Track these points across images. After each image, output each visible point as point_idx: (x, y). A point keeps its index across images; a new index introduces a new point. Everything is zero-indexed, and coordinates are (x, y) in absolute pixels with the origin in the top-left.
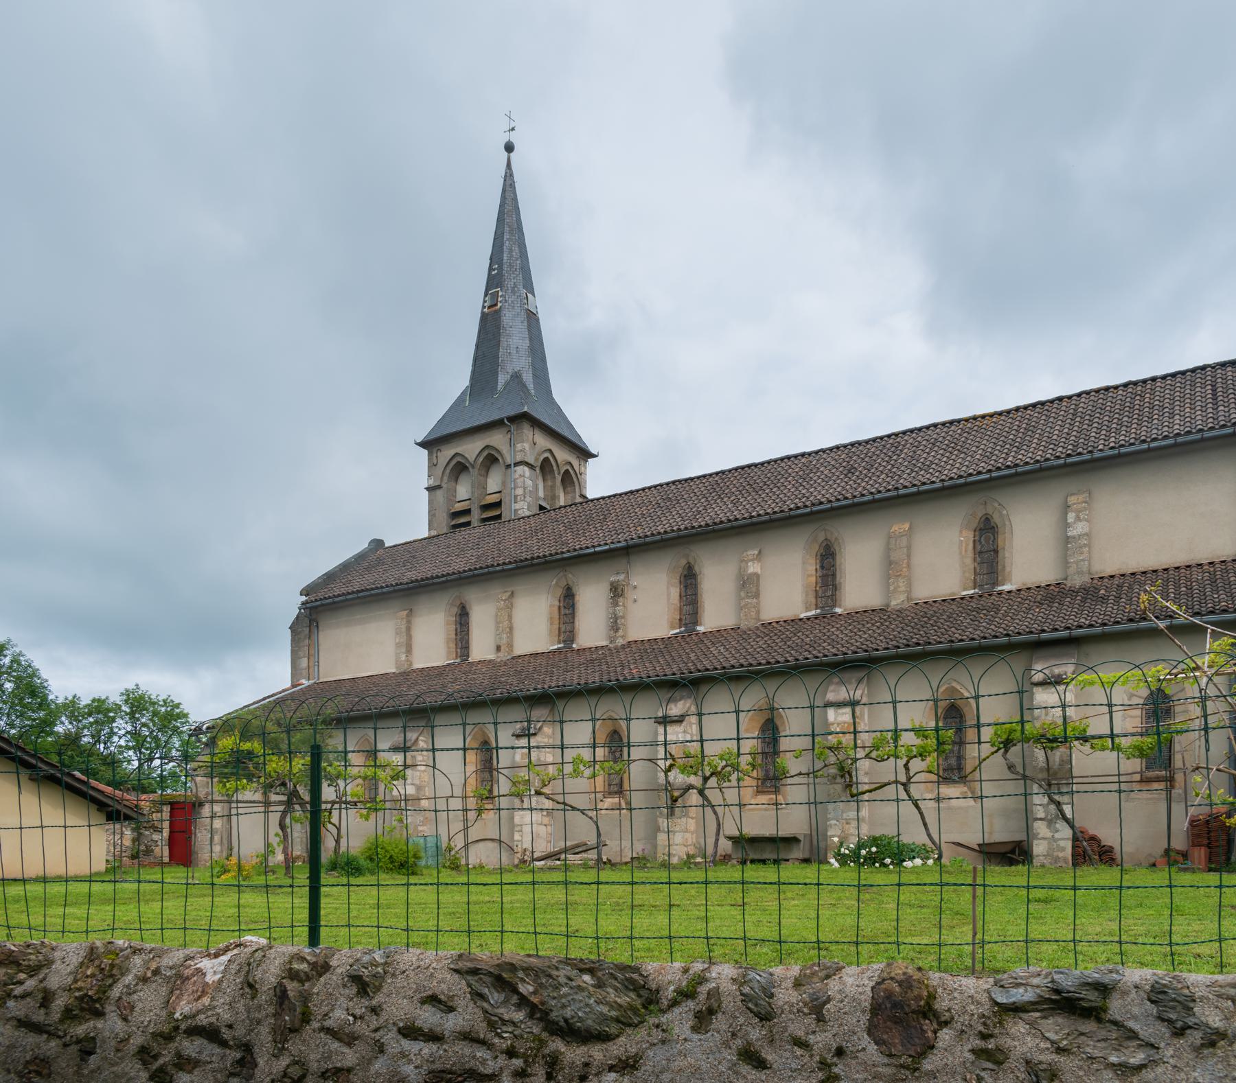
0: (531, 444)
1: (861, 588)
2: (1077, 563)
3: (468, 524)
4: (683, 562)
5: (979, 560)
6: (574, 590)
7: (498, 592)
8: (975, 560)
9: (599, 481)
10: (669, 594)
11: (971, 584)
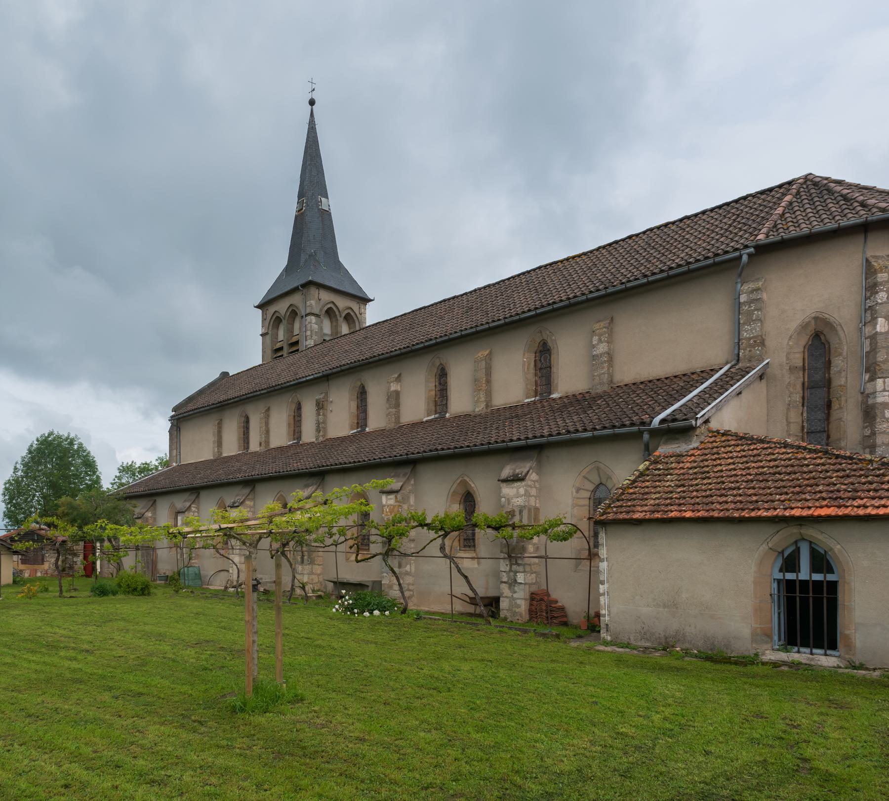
0: (317, 300)
1: (571, 378)
2: (599, 376)
4: (359, 384)
6: (550, 343)
7: (262, 406)
8: (536, 375)
9: (372, 315)
10: (350, 407)
11: (533, 394)
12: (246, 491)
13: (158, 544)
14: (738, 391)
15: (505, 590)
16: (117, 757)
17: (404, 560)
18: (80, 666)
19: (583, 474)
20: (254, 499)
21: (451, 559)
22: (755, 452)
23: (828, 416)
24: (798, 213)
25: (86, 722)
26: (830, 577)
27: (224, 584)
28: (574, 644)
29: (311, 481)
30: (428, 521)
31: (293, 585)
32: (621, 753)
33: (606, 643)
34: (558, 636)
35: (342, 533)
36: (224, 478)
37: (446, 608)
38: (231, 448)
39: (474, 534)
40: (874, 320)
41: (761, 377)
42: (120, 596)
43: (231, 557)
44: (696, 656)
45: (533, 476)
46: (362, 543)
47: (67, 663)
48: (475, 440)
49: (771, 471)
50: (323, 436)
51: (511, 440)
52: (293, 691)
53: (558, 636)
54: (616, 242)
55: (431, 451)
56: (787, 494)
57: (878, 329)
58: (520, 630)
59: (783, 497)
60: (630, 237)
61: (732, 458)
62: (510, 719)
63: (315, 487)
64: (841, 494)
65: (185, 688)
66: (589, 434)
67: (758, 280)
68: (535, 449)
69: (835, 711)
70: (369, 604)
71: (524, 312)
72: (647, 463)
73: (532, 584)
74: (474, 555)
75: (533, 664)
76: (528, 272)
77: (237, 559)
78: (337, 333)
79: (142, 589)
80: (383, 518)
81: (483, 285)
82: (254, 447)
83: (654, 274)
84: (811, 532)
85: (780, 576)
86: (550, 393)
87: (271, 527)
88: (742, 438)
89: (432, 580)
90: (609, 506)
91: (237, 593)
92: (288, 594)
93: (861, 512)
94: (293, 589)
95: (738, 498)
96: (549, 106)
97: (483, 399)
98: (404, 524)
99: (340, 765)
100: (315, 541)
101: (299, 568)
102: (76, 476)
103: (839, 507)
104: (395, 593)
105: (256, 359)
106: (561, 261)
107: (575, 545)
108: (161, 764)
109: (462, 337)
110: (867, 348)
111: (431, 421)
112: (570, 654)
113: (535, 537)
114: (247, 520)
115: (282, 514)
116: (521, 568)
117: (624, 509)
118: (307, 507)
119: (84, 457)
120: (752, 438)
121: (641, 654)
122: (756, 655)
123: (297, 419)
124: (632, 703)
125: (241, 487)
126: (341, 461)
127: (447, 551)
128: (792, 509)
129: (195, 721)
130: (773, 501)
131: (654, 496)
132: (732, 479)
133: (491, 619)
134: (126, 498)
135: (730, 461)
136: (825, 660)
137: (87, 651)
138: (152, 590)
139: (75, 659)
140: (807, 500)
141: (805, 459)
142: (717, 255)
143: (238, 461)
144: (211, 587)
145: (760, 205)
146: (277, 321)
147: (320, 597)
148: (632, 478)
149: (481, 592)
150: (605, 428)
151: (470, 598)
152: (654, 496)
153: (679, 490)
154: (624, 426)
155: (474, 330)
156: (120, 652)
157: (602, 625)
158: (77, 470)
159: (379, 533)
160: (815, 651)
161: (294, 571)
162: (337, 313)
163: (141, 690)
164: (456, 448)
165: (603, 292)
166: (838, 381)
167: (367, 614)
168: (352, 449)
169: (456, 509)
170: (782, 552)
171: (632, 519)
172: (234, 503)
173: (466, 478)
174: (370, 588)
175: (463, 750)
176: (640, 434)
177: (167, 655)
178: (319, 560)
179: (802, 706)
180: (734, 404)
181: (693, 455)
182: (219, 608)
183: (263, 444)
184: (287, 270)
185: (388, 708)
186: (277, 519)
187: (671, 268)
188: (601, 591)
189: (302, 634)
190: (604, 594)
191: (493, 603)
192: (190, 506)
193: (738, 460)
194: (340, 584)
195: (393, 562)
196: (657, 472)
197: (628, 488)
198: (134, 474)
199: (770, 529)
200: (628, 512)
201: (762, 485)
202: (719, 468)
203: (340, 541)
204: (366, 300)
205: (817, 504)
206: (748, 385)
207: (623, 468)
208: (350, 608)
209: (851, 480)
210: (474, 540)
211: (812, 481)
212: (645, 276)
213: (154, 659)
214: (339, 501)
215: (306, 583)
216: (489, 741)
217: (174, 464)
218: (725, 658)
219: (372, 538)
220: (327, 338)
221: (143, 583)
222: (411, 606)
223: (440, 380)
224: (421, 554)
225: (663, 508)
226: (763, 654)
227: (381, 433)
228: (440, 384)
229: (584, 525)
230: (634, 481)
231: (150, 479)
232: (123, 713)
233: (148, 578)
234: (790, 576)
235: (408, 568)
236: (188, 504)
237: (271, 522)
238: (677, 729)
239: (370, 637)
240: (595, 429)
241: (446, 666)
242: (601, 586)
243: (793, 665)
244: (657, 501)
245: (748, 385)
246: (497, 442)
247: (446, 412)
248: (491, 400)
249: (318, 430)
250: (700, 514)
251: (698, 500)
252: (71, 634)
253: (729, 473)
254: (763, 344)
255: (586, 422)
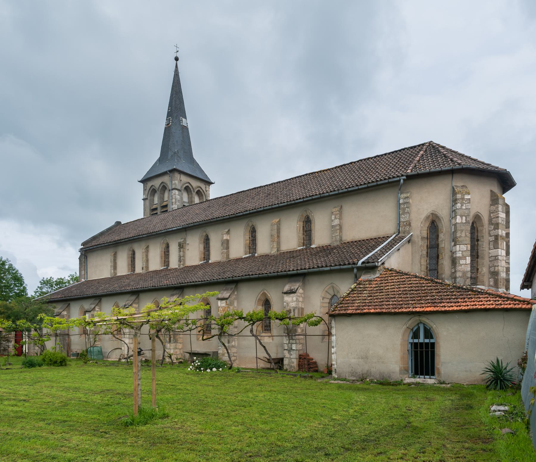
0: (179, 181)
2: (335, 237)
3: (157, 213)
4: (205, 234)
5: (305, 234)
6: (311, 217)
7: (143, 245)
8: (303, 234)
9: (214, 193)
10: (199, 247)
11: (302, 245)
12: (133, 298)
13: (71, 333)
14: (398, 248)
15: (286, 353)
16: (53, 454)
17: (231, 339)
18: (20, 409)
19: (326, 289)
20: (138, 303)
21: (256, 336)
22: (403, 280)
23: (438, 262)
24: (425, 161)
25: (29, 438)
26: (432, 341)
27: (118, 357)
28: (319, 381)
29: (175, 292)
30: (244, 316)
31: (163, 356)
32: (332, 427)
33: (335, 379)
34: (311, 377)
35: (194, 323)
36: (118, 290)
37: (254, 366)
38: (123, 270)
39: (270, 323)
40: (455, 217)
41: (409, 242)
42: (44, 367)
43: (123, 339)
44: (376, 383)
45: (301, 291)
46: (206, 330)
47: (11, 408)
48: (270, 270)
49: (409, 289)
50: (183, 265)
51: (289, 271)
52: (162, 412)
53: (311, 377)
54: (345, 165)
55: (246, 275)
56: (415, 300)
57: (457, 221)
58: (293, 375)
59: (413, 302)
60: (351, 163)
61: (393, 282)
62: (280, 417)
63: (178, 296)
64: (436, 301)
65: (95, 416)
66: (328, 268)
67: (408, 192)
68: (302, 276)
69: (427, 402)
70: (210, 365)
71: (297, 199)
72: (355, 284)
73: (300, 350)
74: (270, 335)
75: (297, 391)
76: (300, 176)
77: (127, 341)
78: (192, 202)
79: (60, 362)
80: (219, 314)
81: (276, 182)
82: (138, 270)
83: (361, 185)
84: (424, 319)
85: (411, 341)
86: (311, 245)
87: (149, 318)
88: (398, 273)
89: (246, 350)
90: (336, 307)
91: (128, 362)
92: (161, 362)
93: (443, 309)
94: (164, 358)
95: (395, 303)
96: (329, 66)
97: (276, 246)
98: (230, 317)
99: (188, 445)
100: (178, 329)
101: (168, 345)
102: (8, 287)
103: (435, 307)
104: (226, 358)
105: (140, 215)
106: (317, 172)
107: (321, 328)
108: (82, 454)
109: (264, 210)
110: (453, 230)
111: (247, 258)
112: (317, 385)
113: (301, 324)
114: (134, 314)
115: (156, 311)
116: (294, 342)
117: (343, 308)
118: (170, 307)
119: (13, 274)
120: (402, 273)
121: (351, 384)
122: (402, 380)
123: (166, 253)
124: (342, 405)
125: (129, 295)
126: (193, 280)
127: (254, 333)
128: (416, 308)
129: (102, 432)
130: (409, 304)
131: (357, 302)
132: (393, 293)
133: (278, 370)
134: (48, 302)
135: (392, 284)
136: (430, 381)
137: (25, 400)
138: (68, 363)
139: (16, 405)
140: (422, 304)
141: (424, 283)
142: (390, 178)
143: (128, 279)
144: (109, 360)
145: (410, 154)
146: (153, 191)
147: (181, 362)
148: (348, 292)
149: (273, 356)
150: (336, 265)
151: (268, 359)
152: (357, 302)
153: (369, 298)
154: (345, 264)
155: (271, 207)
156: (48, 400)
157: (333, 370)
158: (8, 283)
159: (216, 323)
160: (426, 377)
161: (164, 347)
162: (192, 190)
163: (65, 419)
164: (260, 274)
165: (337, 192)
166: (442, 245)
167: (209, 370)
168: (200, 273)
169: (260, 309)
170: (413, 329)
171: (347, 314)
172: (125, 305)
173: (265, 291)
174: (211, 356)
175: (254, 433)
176: (352, 269)
177: (82, 399)
178: (180, 340)
179: (415, 401)
180: (396, 255)
181: (376, 281)
182: (115, 371)
183: (144, 268)
184: (159, 160)
185: (217, 417)
186: (152, 314)
187: (369, 183)
188: (333, 352)
189: (169, 383)
190: (334, 353)
191: (280, 362)
192: (95, 307)
193: (396, 284)
194: (192, 354)
195: (225, 340)
196: (360, 289)
197: (346, 297)
198: (52, 286)
199: (407, 318)
200: (345, 310)
201: (405, 296)
202: (387, 287)
203: (193, 328)
204: (209, 183)
205: (426, 305)
206: (403, 245)
207: (345, 286)
208: (199, 368)
209: (440, 294)
210: (270, 326)
211: (425, 295)
212: (357, 186)
213: (73, 402)
214: (192, 305)
215: (172, 354)
216: (268, 427)
217: (83, 280)
218: (388, 383)
219: (213, 326)
220: (186, 205)
221: (61, 358)
222: (235, 365)
223: (252, 234)
224: (240, 334)
225: (361, 307)
226: (405, 380)
227: (218, 264)
228: (252, 236)
229: (326, 318)
230: (349, 294)
231: (65, 290)
232: (54, 432)
233: (64, 354)
234: (416, 341)
235: (233, 343)
236: (93, 306)
237: (149, 315)
238: (359, 415)
239: (210, 383)
240: (331, 266)
241: (251, 395)
242: (332, 349)
243: (417, 384)
244: (359, 304)
245: (403, 245)
246: (282, 271)
247: (255, 253)
248: (280, 247)
249: (180, 261)
250: (377, 311)
251: (377, 304)
252: (10, 391)
253: (391, 290)
254: (410, 225)
255: (328, 262)
